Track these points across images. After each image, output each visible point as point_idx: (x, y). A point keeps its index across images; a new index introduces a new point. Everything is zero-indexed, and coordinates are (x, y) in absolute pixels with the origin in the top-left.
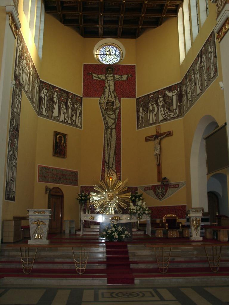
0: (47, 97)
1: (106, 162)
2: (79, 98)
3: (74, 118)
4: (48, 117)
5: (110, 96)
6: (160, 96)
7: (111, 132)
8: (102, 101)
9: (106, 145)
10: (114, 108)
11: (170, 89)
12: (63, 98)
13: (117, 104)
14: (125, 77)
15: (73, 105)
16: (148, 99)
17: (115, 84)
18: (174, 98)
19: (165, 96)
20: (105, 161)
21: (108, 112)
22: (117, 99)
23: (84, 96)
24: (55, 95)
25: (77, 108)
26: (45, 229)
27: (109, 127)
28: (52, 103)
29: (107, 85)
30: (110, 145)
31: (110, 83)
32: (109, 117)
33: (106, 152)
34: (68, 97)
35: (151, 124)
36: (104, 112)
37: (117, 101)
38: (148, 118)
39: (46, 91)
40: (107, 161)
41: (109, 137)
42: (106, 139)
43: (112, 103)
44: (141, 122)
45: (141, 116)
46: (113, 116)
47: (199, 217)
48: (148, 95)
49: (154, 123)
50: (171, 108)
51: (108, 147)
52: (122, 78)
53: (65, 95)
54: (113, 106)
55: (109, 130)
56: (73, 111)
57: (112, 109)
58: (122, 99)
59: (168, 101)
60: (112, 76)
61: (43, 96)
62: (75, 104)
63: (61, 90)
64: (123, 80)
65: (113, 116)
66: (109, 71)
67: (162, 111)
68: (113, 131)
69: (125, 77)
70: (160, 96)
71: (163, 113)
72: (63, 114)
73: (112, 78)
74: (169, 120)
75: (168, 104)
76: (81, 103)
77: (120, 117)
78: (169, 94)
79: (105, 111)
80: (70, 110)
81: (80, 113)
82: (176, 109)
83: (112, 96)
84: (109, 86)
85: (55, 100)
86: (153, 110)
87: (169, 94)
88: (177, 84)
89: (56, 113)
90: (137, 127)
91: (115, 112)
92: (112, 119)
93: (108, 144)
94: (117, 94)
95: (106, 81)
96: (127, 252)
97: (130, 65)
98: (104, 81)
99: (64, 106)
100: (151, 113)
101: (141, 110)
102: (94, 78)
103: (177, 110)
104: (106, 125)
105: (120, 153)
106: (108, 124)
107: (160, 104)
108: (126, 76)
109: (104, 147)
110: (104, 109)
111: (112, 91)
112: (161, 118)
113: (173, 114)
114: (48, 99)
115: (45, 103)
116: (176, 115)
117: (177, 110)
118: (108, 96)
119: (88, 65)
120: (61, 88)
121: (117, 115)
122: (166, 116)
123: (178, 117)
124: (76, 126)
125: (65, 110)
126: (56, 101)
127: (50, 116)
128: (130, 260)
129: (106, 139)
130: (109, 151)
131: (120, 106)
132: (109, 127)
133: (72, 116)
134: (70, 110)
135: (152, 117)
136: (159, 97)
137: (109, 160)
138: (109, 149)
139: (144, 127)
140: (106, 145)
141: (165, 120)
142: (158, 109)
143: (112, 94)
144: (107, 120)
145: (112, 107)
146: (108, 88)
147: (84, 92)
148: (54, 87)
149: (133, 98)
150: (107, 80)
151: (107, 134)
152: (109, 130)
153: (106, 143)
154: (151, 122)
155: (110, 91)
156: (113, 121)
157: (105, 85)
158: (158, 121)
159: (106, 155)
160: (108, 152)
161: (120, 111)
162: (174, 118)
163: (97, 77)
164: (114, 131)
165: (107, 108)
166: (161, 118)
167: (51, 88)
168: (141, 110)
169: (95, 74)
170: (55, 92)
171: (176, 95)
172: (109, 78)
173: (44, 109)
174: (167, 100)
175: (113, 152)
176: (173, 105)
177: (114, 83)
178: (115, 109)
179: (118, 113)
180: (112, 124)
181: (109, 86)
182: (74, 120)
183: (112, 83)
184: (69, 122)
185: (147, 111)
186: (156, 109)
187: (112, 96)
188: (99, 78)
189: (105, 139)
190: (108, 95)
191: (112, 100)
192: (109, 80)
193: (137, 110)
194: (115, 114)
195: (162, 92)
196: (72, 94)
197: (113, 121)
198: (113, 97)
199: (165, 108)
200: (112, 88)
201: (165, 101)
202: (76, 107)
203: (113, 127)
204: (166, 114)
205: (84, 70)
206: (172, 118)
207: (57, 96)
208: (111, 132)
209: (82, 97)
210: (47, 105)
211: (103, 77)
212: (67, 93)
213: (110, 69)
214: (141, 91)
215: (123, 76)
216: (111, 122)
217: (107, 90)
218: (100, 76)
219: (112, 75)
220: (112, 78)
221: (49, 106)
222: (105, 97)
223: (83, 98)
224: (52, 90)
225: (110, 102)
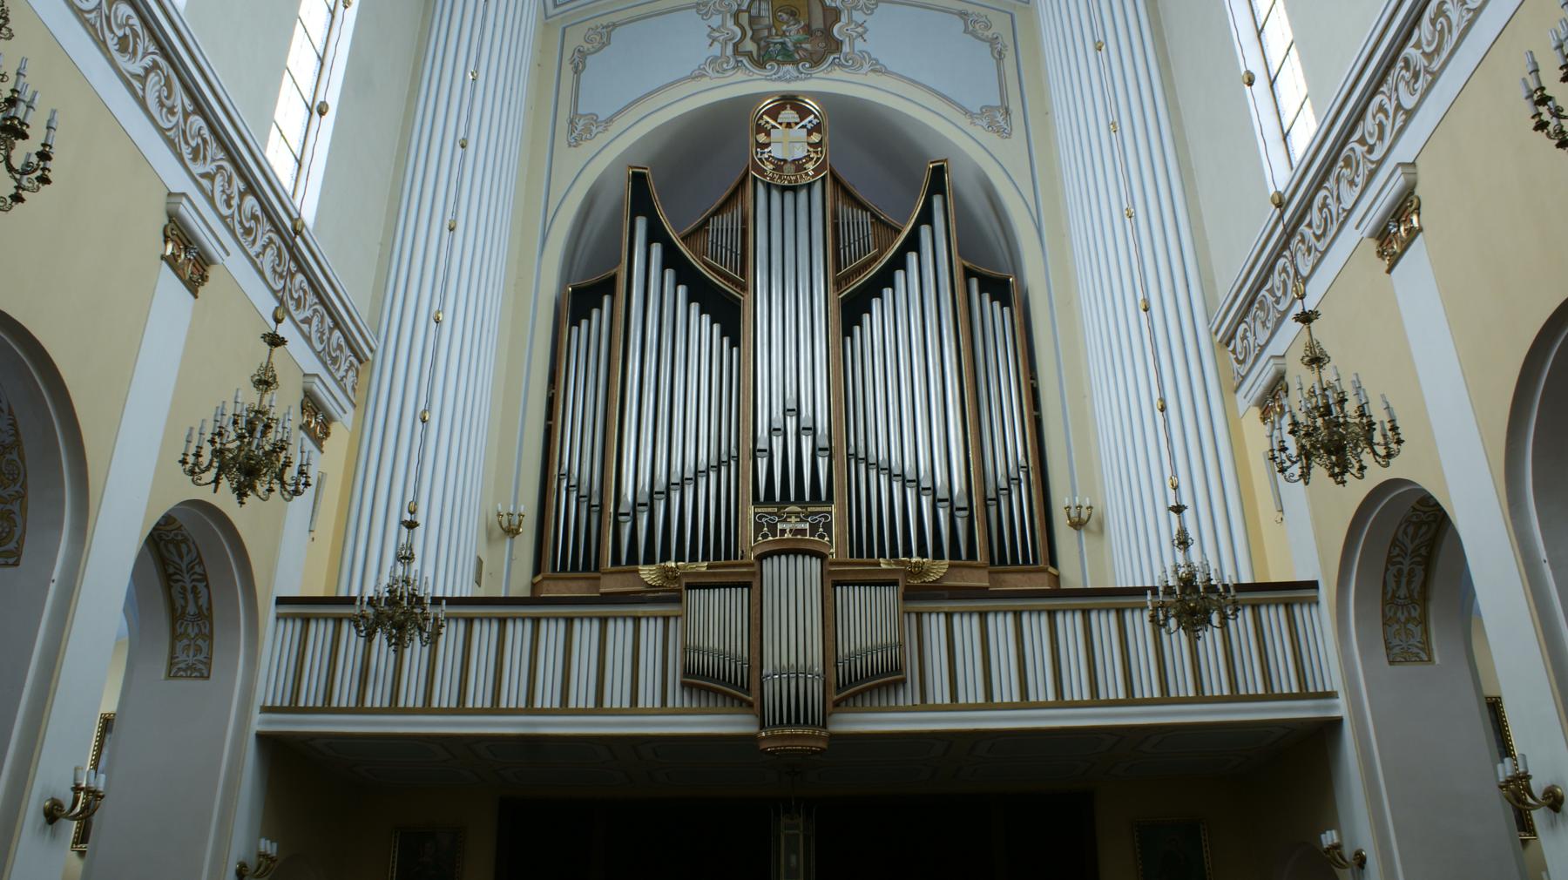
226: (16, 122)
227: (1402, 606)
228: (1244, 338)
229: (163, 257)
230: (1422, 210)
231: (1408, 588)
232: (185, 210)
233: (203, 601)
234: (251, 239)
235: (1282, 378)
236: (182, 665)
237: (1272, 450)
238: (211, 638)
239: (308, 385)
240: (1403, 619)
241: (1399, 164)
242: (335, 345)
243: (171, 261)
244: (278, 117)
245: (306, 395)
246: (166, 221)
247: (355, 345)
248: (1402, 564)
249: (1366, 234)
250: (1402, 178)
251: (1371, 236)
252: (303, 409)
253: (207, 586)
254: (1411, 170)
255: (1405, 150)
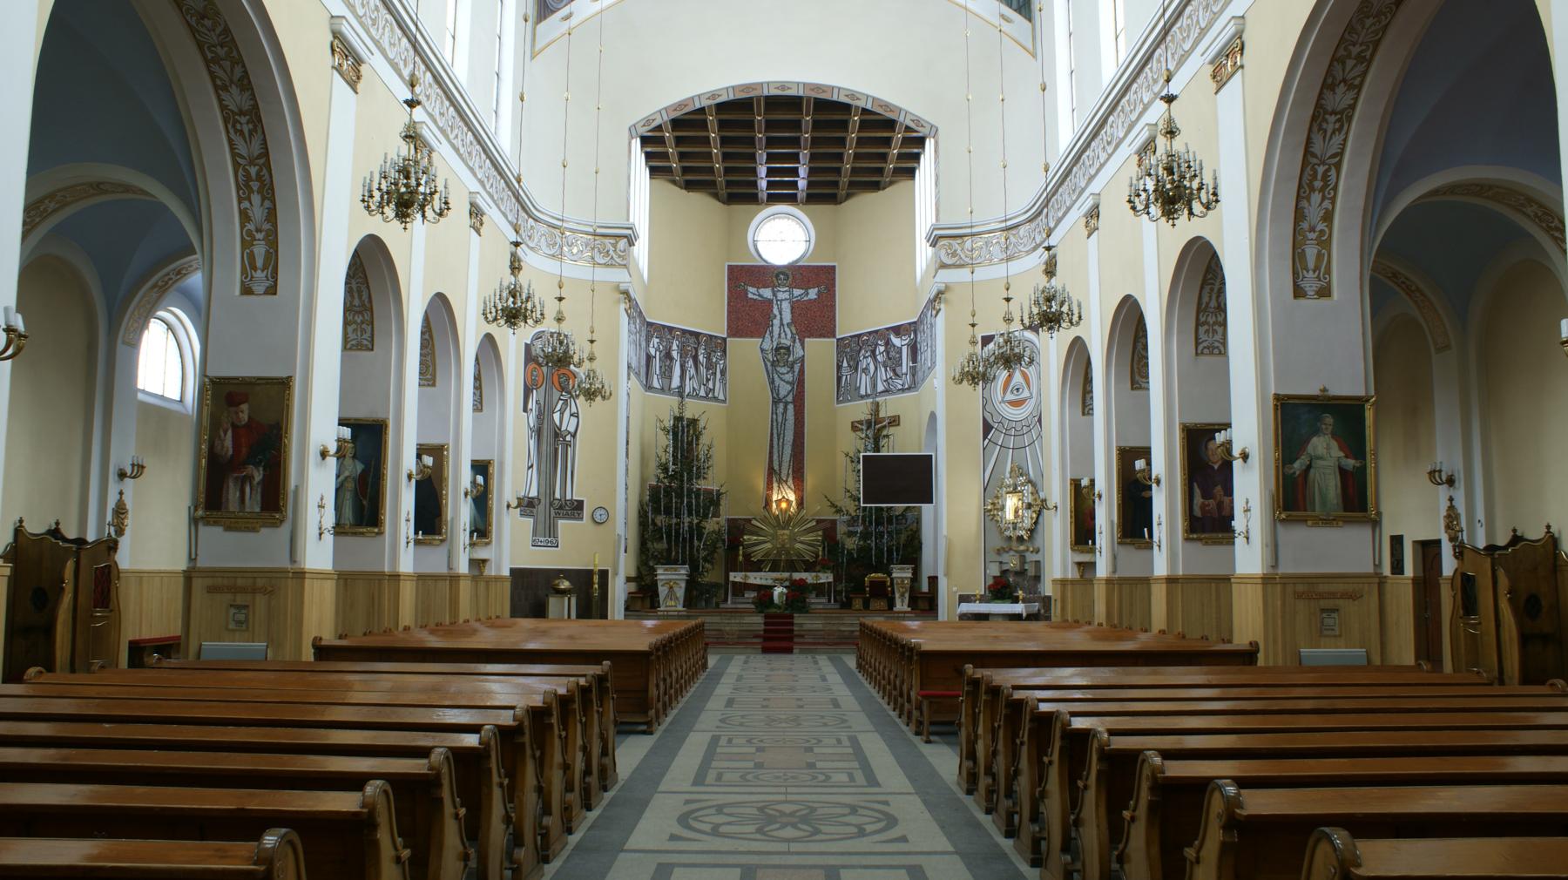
0: (660, 352)
1: (775, 471)
2: (719, 341)
3: (710, 385)
4: (662, 390)
5: (783, 335)
6: (879, 342)
7: (785, 409)
8: (767, 345)
9: (775, 435)
10: (791, 359)
11: (897, 330)
12: (689, 348)
13: (798, 351)
14: (813, 294)
15: (708, 358)
16: (858, 344)
17: (792, 308)
18: (905, 349)
19: (888, 343)
20: (773, 469)
21: (778, 369)
22: (797, 341)
23: (729, 336)
24: (674, 344)
25: (716, 363)
26: (680, 592)
27: (780, 400)
28: (669, 362)
29: (776, 311)
30: (782, 435)
31: (783, 306)
32: (781, 379)
33: (775, 450)
34: (699, 343)
35: (862, 397)
36: (770, 368)
37: (798, 344)
38: (858, 385)
39: (658, 340)
40: (776, 467)
41: (780, 420)
42: (775, 424)
43: (788, 349)
44: (845, 391)
45: (844, 377)
46: (789, 377)
47: (906, 578)
48: (859, 336)
49: (867, 396)
50: (898, 369)
51: (779, 439)
52: (808, 294)
53: (693, 339)
54: (789, 356)
55: (781, 406)
56: (708, 369)
57: (787, 361)
58: (807, 340)
59: (893, 354)
60: (786, 291)
61: (652, 351)
62: (713, 354)
63: (684, 332)
64: (810, 300)
65: (789, 377)
66: (780, 279)
67: (882, 374)
68: (788, 407)
69: (813, 294)
70: (879, 342)
71: (885, 378)
72: (690, 379)
73: (786, 295)
74: (894, 393)
75: (893, 363)
76: (724, 351)
77: (804, 379)
78: (896, 341)
79: (772, 365)
80: (703, 370)
81: (723, 372)
82: (907, 374)
83: (786, 335)
84: (781, 314)
85: (675, 354)
86: (866, 369)
87: (896, 341)
88: (910, 324)
89: (676, 382)
90: (838, 399)
91: (792, 368)
92: (788, 382)
93: (779, 435)
94: (797, 329)
95: (775, 302)
96: (792, 624)
97: (825, 267)
98: (770, 301)
99: (691, 362)
100: (863, 374)
101: (845, 364)
102: (750, 296)
103: (908, 376)
104: (775, 395)
105: (802, 453)
106: (778, 395)
107: (878, 357)
108: (817, 289)
109: (772, 440)
110: (769, 360)
111: (787, 324)
112: (880, 388)
113: (901, 382)
114: (662, 355)
115: (657, 364)
116: (906, 386)
117: (908, 376)
118: (780, 334)
119: (737, 266)
120: (683, 328)
121: (796, 374)
122: (889, 384)
123: (909, 389)
124: (716, 399)
125: (693, 371)
126: (675, 357)
127: (666, 388)
128: (795, 633)
129: (775, 424)
130: (781, 449)
131: (803, 356)
132: (780, 400)
133: (708, 380)
134: (703, 370)
135: (864, 383)
136: (877, 345)
137: (780, 465)
138: (781, 444)
139: (850, 401)
140: (775, 435)
141: (887, 391)
142: (876, 368)
143: (787, 330)
144: (777, 385)
145: (786, 357)
146: (778, 317)
147: (729, 327)
148: (671, 329)
149: (829, 337)
150: (777, 301)
151: (776, 414)
152: (781, 406)
153: (775, 431)
154: (863, 392)
155: (782, 324)
156: (789, 387)
157: (772, 311)
158: (875, 393)
159: (775, 457)
160: (779, 451)
161: (802, 366)
162: (903, 390)
163: (754, 294)
164: (791, 407)
165: (778, 360)
166: (880, 388)
167: (665, 331)
168: (845, 364)
169: (753, 287)
170: (674, 338)
171: (908, 345)
172: (780, 296)
173: (655, 376)
174: (892, 354)
175: (788, 450)
176: (901, 365)
177: (791, 306)
178: (794, 363)
179: (799, 372)
180: (786, 394)
181: (781, 314)
182: (710, 389)
183: (786, 306)
184: (702, 393)
185: (856, 369)
186: (872, 368)
187: (786, 335)
188: (760, 295)
189: (772, 425)
190: (778, 332)
191: (787, 342)
192: (782, 300)
193: (838, 364)
194: (794, 372)
195: (882, 335)
196: (705, 335)
197: (789, 387)
198: (789, 336)
199: (888, 369)
200: (787, 317)
201: (888, 353)
202: (714, 360)
203: (790, 398)
204: (890, 381)
205: (729, 279)
206: (899, 390)
207: (678, 346)
208: (785, 409)
209: (725, 336)
210: (661, 367)
211: (767, 293)
212: (697, 335)
213: (782, 276)
214: (849, 323)
215: (810, 291)
216: (784, 389)
217: (776, 322)
218: (762, 291)
219: (787, 288)
220: (786, 295)
221: (663, 370)
222: (772, 337)
223: (728, 339)
224: (669, 337)
225: (781, 348)
226: (565, 341)
227: (1212, 313)
228: (1136, 92)
229: (333, 67)
230: (1245, 51)
231: (1217, 301)
232: (346, 30)
233: (365, 297)
234: (376, 27)
235: (1097, 207)
236: (353, 342)
237: (1130, 196)
238: (372, 323)
239: (473, 200)
240: (1211, 322)
241: (1147, 124)
242: (373, 8)
243: (338, 69)
244: (876, 735)
245: (335, 37)
246: (330, 38)
247: (490, 154)
248: (1213, 284)
249: (1133, 151)
250: (1147, 133)
251: (1136, 153)
252: (471, 214)
253: (368, 287)
254: (1097, 197)
255: (1095, 187)
